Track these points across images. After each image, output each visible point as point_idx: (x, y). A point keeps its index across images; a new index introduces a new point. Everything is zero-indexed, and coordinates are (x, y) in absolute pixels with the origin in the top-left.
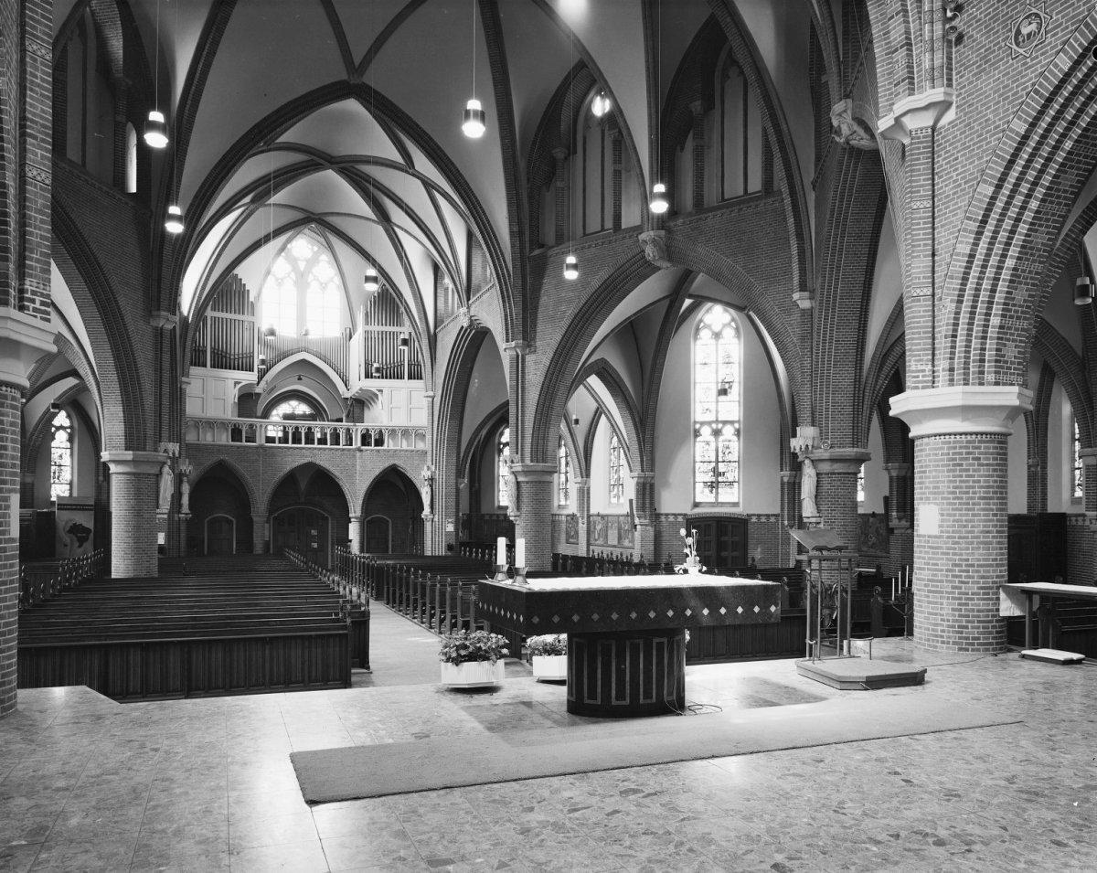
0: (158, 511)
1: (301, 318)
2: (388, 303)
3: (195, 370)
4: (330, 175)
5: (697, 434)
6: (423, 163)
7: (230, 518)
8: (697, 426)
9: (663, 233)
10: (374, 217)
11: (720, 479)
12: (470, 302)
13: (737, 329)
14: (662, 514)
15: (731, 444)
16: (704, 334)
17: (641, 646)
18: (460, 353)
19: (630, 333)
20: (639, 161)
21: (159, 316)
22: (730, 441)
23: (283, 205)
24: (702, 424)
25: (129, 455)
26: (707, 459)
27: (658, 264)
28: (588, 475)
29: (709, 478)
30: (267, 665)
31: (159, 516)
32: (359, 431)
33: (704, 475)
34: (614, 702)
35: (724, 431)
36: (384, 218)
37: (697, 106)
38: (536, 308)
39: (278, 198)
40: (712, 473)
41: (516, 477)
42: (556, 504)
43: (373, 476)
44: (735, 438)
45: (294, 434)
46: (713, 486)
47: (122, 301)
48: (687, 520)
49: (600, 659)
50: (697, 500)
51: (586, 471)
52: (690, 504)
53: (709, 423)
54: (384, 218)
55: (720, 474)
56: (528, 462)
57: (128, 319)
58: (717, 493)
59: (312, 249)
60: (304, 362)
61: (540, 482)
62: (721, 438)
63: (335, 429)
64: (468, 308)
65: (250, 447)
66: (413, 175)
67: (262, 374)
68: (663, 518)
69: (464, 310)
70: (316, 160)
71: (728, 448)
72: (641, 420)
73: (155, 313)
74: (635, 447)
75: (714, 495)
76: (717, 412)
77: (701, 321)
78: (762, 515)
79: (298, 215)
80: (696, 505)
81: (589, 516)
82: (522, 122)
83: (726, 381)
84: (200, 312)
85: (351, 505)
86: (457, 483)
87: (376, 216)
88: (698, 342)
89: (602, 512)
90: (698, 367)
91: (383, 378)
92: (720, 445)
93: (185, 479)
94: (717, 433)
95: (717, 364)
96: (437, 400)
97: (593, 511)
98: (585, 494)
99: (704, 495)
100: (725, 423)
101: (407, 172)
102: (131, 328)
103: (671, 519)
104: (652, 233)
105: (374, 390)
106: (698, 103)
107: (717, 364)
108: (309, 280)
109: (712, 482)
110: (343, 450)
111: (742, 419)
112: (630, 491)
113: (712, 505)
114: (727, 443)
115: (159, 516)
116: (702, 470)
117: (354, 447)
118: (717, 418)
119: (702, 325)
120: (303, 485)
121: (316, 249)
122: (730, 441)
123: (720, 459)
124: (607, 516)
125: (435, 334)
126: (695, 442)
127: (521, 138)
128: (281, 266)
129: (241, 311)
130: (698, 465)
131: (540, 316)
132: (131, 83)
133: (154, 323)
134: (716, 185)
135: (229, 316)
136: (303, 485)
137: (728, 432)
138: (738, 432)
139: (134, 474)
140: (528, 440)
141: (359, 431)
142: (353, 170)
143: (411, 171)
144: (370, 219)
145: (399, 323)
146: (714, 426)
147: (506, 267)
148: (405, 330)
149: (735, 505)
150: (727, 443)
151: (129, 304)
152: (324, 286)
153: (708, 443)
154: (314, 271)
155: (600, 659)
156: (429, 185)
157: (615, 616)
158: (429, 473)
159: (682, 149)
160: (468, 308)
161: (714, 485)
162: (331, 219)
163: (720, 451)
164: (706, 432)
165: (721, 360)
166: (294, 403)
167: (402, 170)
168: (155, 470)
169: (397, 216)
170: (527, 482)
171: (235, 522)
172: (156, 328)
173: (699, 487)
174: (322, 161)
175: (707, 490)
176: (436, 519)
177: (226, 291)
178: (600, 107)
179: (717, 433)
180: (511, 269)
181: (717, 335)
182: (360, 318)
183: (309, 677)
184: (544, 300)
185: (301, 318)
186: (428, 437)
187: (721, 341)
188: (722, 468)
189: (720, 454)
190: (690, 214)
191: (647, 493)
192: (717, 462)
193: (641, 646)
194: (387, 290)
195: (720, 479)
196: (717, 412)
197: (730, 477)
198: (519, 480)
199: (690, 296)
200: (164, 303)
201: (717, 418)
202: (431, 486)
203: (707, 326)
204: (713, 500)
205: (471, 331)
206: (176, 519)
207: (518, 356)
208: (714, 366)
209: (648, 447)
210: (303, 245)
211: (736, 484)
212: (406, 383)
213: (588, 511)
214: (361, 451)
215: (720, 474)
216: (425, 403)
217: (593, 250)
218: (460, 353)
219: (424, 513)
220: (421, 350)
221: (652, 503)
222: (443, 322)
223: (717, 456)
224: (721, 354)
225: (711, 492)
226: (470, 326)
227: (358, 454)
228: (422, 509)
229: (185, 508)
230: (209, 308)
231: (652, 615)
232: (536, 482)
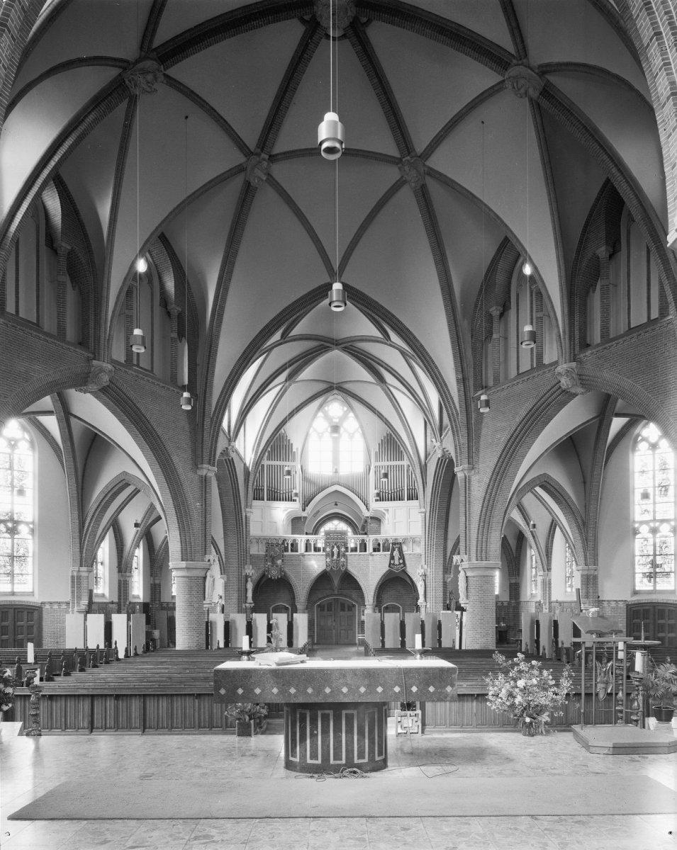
0: (204, 602)
1: (336, 461)
2: (392, 444)
3: (256, 503)
4: (336, 353)
5: (635, 532)
6: (394, 338)
7: (287, 606)
8: (636, 525)
9: (574, 364)
10: (373, 381)
11: (658, 570)
12: (442, 437)
13: (32, 443)
14: (604, 601)
15: (668, 539)
16: (643, 446)
17: (331, 717)
18: (441, 478)
19: (570, 448)
20: (553, 307)
21: (202, 468)
22: (666, 537)
23: (308, 380)
24: (642, 523)
25: (184, 564)
26: (645, 553)
27: (573, 391)
28: (549, 570)
29: (647, 569)
30: (196, 714)
31: (205, 606)
32: (371, 541)
33: (641, 568)
34: (309, 761)
35: (661, 528)
36: (381, 379)
37: (602, 251)
38: (479, 437)
39: (307, 373)
40: (650, 565)
41: (465, 572)
42: (529, 594)
43: (382, 574)
44: (30, 537)
45: (292, 545)
46: (651, 576)
47: (175, 459)
48: (627, 605)
49: (298, 724)
50: (637, 588)
51: (548, 567)
52: (629, 592)
53: (647, 522)
54: (381, 379)
55: (657, 566)
56: (474, 561)
57: (180, 470)
58: (655, 582)
59: (343, 409)
60: (336, 491)
61: (484, 576)
62: (658, 535)
63: (363, 540)
64: (441, 442)
65: (293, 556)
66: (391, 345)
67: (305, 504)
68: (605, 604)
69: (439, 444)
70: (323, 344)
71: (664, 543)
72: (584, 523)
73: (199, 466)
74: (579, 545)
75: (652, 584)
76: (654, 512)
77: (638, 435)
78: (63, 603)
79: (322, 386)
80: (636, 593)
81: (550, 603)
82: (462, 291)
83: (662, 485)
84: (258, 463)
85: (366, 599)
86: (444, 577)
87: (375, 379)
88: (637, 454)
89: (560, 600)
90: (637, 475)
91: (380, 500)
92: (658, 541)
93: (249, 579)
94: (654, 531)
95: (654, 471)
96: (428, 514)
97: (553, 599)
98: (547, 585)
99: (642, 585)
100: (662, 521)
101: (386, 344)
102: (183, 477)
103: (613, 604)
104: (565, 366)
105: (382, 510)
106: (603, 248)
107: (654, 471)
108: (25, 434)
109: (651, 573)
110: (359, 555)
111: (37, 521)
112: (577, 582)
113: (649, 592)
114: (664, 539)
115: (205, 606)
116: (641, 562)
117: (367, 553)
118: (654, 517)
119: (640, 438)
120: (336, 582)
121: (345, 409)
122: (666, 537)
123: (658, 553)
124: (564, 602)
125: (426, 465)
126: (634, 538)
127: (462, 302)
128: (320, 424)
129: (287, 459)
130: (637, 559)
131: (482, 443)
132: (180, 310)
133: (200, 473)
134: (623, 316)
135: (278, 463)
136: (336, 582)
137: (665, 529)
138: (32, 531)
139: (188, 577)
140: (474, 542)
141: (371, 541)
142: (352, 348)
143: (389, 342)
144: (369, 382)
145: (401, 459)
146: (652, 525)
147: (455, 408)
148: (405, 462)
149: (32, 594)
150: (664, 539)
151: (181, 461)
152: (351, 436)
153: (646, 540)
154: (314, 425)
155: (298, 724)
156: (403, 353)
157: (293, 691)
158: (422, 571)
159: (594, 291)
160: (441, 442)
161: (652, 575)
162: (347, 386)
163: (658, 545)
164: (644, 530)
165: (657, 467)
166: (336, 522)
167: (382, 343)
168: (202, 574)
169: (389, 378)
170: (474, 577)
171: (290, 608)
172: (201, 476)
173: (638, 577)
174: (328, 345)
175: (645, 580)
176: (428, 606)
177: (276, 445)
178: (528, 270)
179: (654, 531)
180: (458, 410)
181: (654, 446)
182: (373, 460)
183: (105, 725)
184: (484, 431)
185: (336, 461)
186: (423, 543)
187: (658, 451)
188: (659, 560)
189: (658, 549)
190: (598, 345)
191: (590, 582)
192: (655, 555)
193: (331, 717)
194: (391, 435)
195: (658, 570)
196: (654, 512)
197: (667, 568)
198: (468, 575)
199: (618, 415)
200: (206, 458)
201: (654, 517)
202: (425, 581)
203: (644, 439)
204: (652, 588)
205: (446, 460)
206: (244, 606)
207: (465, 477)
208: (651, 473)
209: (591, 544)
210: (336, 407)
211: (672, 575)
212: (405, 503)
213: (550, 598)
214: (373, 555)
215: (657, 566)
216: (420, 518)
217: (520, 386)
218: (441, 478)
219: (419, 601)
220: (417, 480)
221: (596, 591)
222: (429, 454)
223: (655, 550)
224: (658, 462)
225: (650, 581)
226: (443, 456)
227: (371, 558)
228: (417, 599)
229: (250, 599)
230: (265, 458)
231: (328, 690)
232: (481, 576)
